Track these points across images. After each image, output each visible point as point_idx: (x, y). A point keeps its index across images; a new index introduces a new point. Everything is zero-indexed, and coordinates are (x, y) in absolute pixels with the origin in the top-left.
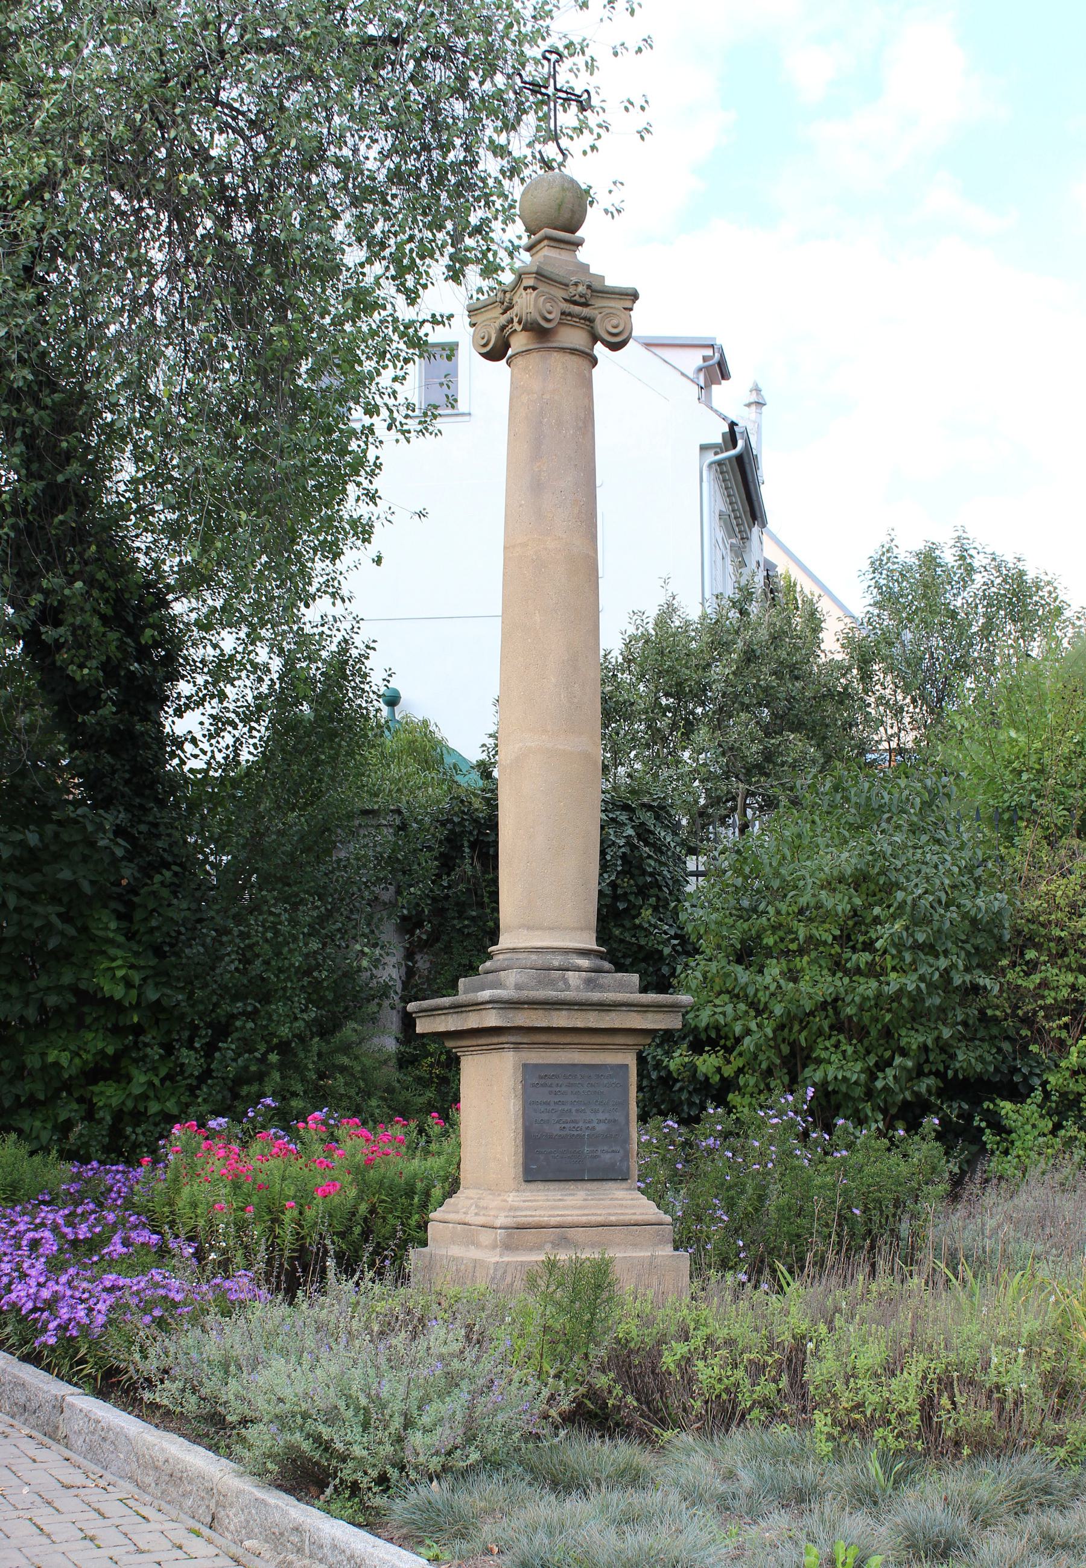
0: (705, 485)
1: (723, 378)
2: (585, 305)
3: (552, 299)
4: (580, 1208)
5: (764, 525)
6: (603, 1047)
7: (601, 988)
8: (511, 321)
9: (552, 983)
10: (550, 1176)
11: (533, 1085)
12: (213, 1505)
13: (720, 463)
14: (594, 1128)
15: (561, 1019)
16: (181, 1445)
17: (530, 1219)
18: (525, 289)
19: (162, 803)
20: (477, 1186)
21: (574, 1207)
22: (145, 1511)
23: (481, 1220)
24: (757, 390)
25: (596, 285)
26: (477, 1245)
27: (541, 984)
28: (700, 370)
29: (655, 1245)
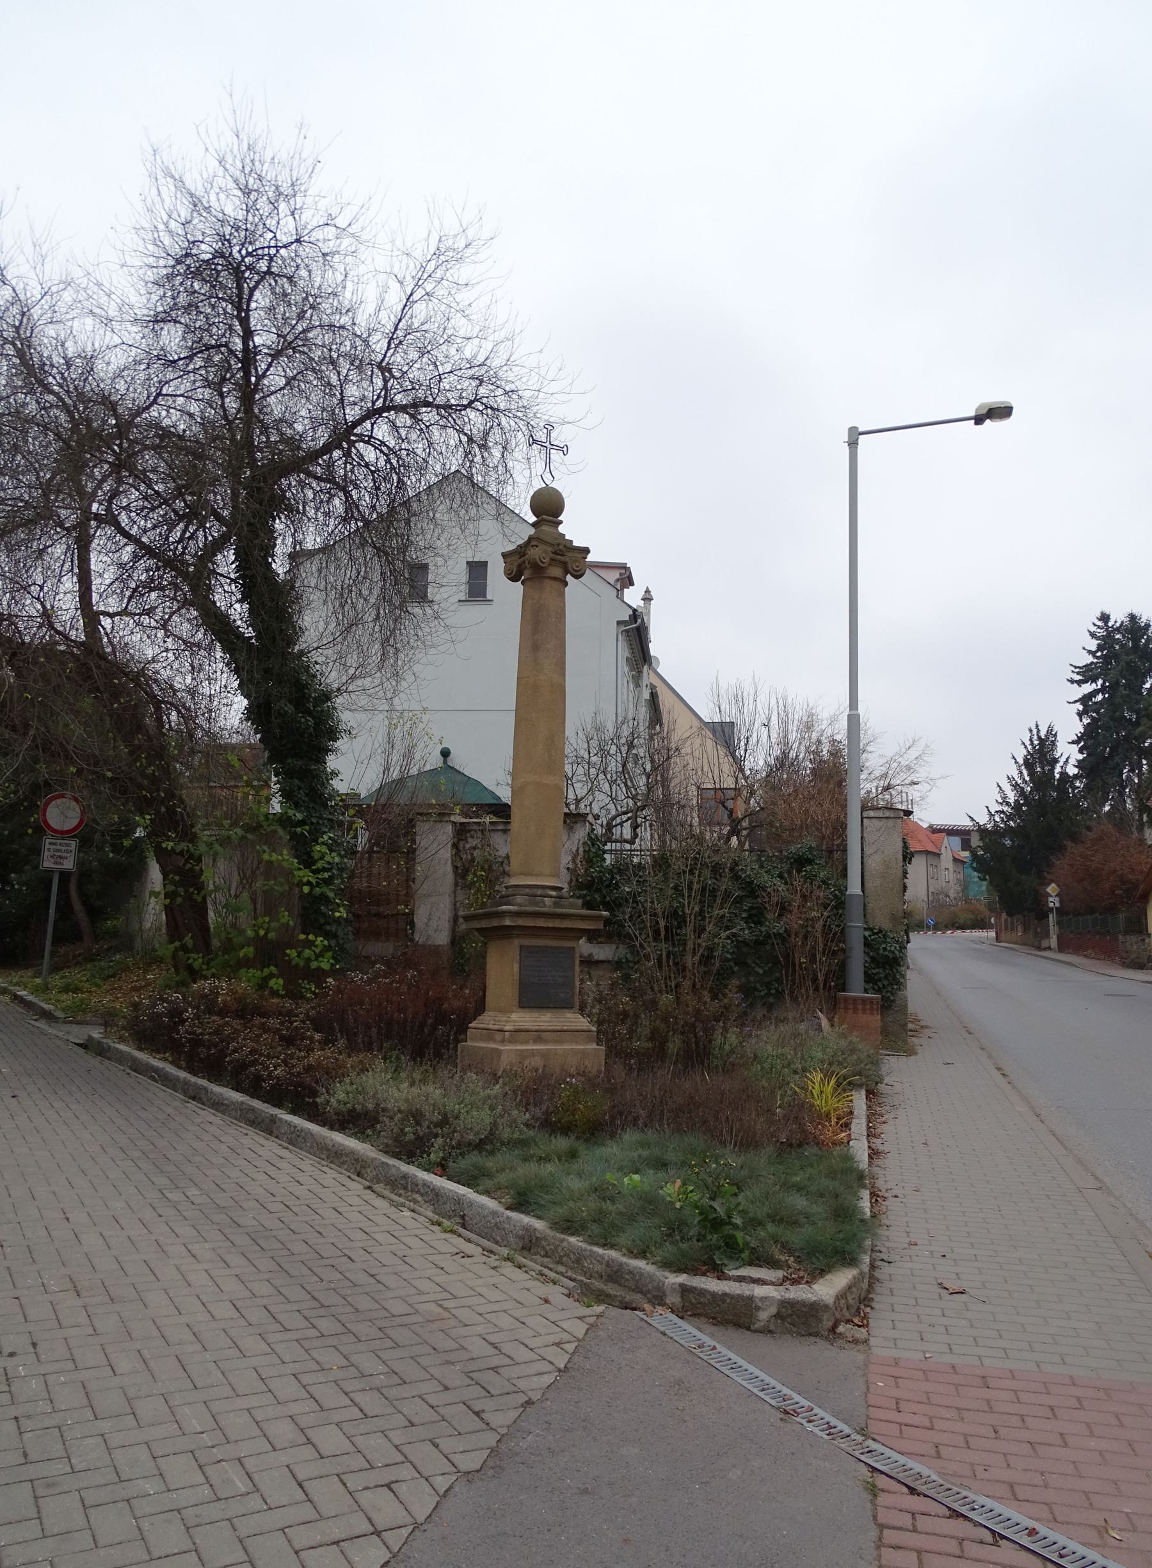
3: (545, 552)
5: (650, 664)
9: (536, 904)
12: (358, 1167)
13: (627, 631)
15: (541, 923)
22: (324, 1169)
23: (496, 1027)
24: (647, 591)
26: (494, 1041)
29: (587, 1043)
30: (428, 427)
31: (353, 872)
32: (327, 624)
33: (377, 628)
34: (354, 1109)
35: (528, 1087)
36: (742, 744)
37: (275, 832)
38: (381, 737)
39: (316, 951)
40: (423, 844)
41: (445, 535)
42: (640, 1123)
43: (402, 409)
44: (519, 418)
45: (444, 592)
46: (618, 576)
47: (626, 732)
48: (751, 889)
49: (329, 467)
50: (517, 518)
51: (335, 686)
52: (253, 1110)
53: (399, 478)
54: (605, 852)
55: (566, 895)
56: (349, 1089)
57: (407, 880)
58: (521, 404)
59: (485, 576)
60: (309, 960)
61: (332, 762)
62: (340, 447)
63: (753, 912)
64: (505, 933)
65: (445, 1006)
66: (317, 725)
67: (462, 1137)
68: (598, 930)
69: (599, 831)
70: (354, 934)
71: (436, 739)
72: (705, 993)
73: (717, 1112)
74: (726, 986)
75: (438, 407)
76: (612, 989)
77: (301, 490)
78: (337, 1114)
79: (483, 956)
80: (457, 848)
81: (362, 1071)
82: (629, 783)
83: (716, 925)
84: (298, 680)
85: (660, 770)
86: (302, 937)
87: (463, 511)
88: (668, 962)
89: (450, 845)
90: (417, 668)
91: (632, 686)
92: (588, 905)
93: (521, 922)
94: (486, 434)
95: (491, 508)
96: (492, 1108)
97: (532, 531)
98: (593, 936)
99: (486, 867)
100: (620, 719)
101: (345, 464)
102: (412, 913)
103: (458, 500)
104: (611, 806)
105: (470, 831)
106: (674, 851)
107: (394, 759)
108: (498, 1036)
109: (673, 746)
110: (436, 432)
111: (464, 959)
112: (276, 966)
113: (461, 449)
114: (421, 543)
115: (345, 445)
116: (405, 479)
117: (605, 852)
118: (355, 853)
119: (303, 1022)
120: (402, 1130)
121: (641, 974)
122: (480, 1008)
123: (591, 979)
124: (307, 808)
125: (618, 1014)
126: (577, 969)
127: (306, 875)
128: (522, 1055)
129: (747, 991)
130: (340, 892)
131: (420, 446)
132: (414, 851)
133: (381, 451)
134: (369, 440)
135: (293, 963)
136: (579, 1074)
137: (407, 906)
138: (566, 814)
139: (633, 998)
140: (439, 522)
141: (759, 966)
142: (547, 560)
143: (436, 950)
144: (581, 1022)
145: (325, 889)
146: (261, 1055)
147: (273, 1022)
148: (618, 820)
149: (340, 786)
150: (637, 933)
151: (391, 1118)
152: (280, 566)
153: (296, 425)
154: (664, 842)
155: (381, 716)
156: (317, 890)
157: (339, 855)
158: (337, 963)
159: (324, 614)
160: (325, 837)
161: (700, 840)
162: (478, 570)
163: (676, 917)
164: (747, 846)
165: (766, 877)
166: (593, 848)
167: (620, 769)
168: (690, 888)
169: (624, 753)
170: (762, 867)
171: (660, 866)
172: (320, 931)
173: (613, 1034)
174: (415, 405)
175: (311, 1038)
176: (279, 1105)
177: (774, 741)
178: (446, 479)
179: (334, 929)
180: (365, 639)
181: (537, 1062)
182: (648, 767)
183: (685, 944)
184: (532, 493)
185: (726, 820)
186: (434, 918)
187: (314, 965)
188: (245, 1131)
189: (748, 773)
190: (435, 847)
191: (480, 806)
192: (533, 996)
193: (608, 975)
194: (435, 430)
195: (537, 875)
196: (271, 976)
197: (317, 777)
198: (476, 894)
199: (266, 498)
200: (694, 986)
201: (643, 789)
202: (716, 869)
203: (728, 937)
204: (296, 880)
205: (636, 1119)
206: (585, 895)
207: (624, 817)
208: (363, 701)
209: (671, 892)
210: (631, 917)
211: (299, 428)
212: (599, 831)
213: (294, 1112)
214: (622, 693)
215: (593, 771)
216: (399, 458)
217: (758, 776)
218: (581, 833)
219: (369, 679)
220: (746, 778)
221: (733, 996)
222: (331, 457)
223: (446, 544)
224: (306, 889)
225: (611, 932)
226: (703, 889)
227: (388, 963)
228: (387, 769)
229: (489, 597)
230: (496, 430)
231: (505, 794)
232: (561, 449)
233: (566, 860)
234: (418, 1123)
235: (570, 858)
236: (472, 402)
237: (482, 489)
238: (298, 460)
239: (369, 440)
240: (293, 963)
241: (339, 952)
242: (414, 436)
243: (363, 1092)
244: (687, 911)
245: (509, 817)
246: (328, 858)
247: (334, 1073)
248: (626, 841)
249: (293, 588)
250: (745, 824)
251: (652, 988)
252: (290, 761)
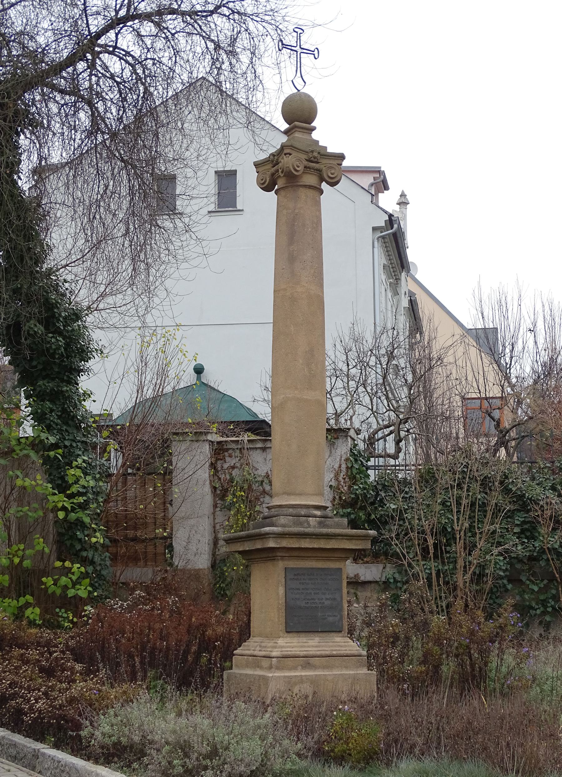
0: (376, 250)
1: (385, 189)
3: (299, 160)
4: (316, 647)
5: (408, 271)
6: (328, 559)
7: (328, 526)
8: (277, 171)
9: (301, 524)
10: (300, 630)
11: (291, 579)
13: (383, 237)
14: (324, 603)
15: (306, 544)
16: (107, 772)
17: (289, 653)
18: (285, 154)
19: (78, 428)
20: (260, 635)
21: (313, 646)
24: (403, 195)
25: (322, 152)
26: (261, 668)
27: (296, 524)
28: (372, 185)
29: (357, 667)
30: (173, 35)
31: (108, 495)
32: (76, 241)
33: (127, 243)
34: (120, 742)
35: (298, 715)
36: (507, 350)
37: (27, 456)
38: (134, 355)
39: (72, 578)
40: (179, 465)
41: (195, 145)
42: (417, 750)
43: (148, 17)
44: (267, 22)
45: (195, 204)
46: (372, 181)
47: (385, 342)
48: (523, 503)
49: (73, 80)
50: (268, 126)
51: (85, 304)
52: (15, 745)
53: (146, 89)
54: (368, 468)
55: (330, 514)
56: (114, 721)
57: (164, 503)
58: (268, 8)
60: (66, 587)
61: (85, 383)
62: (83, 58)
63: (526, 526)
64: (269, 555)
65: (209, 632)
66: (67, 345)
67: (233, 768)
68: (364, 550)
69: (361, 446)
70: (111, 560)
71: (190, 356)
72: (479, 612)
73: (498, 737)
74: (500, 605)
75: (183, 14)
76: (381, 612)
77: (50, 106)
78: (102, 747)
79: (246, 579)
80: (215, 468)
81: (127, 701)
82: (390, 395)
83: (487, 541)
84: (47, 300)
85: (422, 382)
86: (58, 564)
87: (212, 120)
88: (438, 581)
89: (207, 464)
90: (168, 283)
91: (389, 294)
92: (353, 524)
93: (285, 543)
94: (233, 40)
95: (241, 116)
96: (263, 738)
97: (284, 139)
98: (358, 556)
99: (246, 486)
100: (379, 329)
101: (90, 75)
102: (170, 537)
103: (206, 109)
104: (372, 420)
105: (227, 450)
106: (441, 465)
107: (148, 378)
108: (265, 663)
109: (435, 355)
110: (182, 40)
111: (226, 584)
112: (32, 595)
113: (208, 57)
114: (171, 155)
115: (89, 56)
116: (152, 89)
117: (368, 468)
118: (110, 475)
119: (63, 652)
120: (170, 763)
121: (411, 594)
122: (245, 633)
123: (358, 602)
124: (60, 431)
125: (388, 637)
126: (345, 590)
127: (60, 500)
128: (290, 682)
129: (523, 609)
130: (96, 517)
131: (167, 54)
132: (171, 472)
133: (127, 62)
134: (114, 50)
135: (50, 591)
136: (350, 700)
137: (165, 529)
138: (328, 430)
139: (404, 620)
140: (187, 132)
141: (533, 583)
142: (300, 169)
143: (196, 575)
144: (352, 647)
145: (80, 514)
146: (21, 687)
147: (33, 654)
148: (380, 434)
149: (92, 407)
150: (405, 552)
151: (158, 750)
152: (25, 183)
153: (38, 38)
154: (428, 456)
155: (133, 334)
156: (73, 516)
157: (94, 478)
158: (95, 589)
159: (72, 231)
160: (80, 460)
161: (467, 453)
162: (227, 179)
163: (446, 535)
164: (515, 459)
165: (539, 490)
166: (356, 464)
167: (381, 381)
168: (459, 504)
169: (384, 364)
170: (533, 479)
171: (427, 482)
172: (77, 557)
173: (384, 658)
174: (160, 13)
175: (72, 669)
176: (41, 738)
177: (540, 347)
178: (193, 86)
179: (90, 556)
180: (114, 255)
181: (307, 689)
182: (410, 378)
183: (456, 562)
184: (283, 99)
185: (493, 431)
186: (194, 542)
187: (71, 593)
188: (7, 767)
189: (514, 380)
190: (192, 467)
191: (237, 424)
192: (300, 620)
193: (375, 596)
194: (180, 37)
195: (300, 495)
196: (27, 605)
197: (69, 398)
198: (235, 515)
199: (11, 114)
200: (467, 606)
201: (405, 401)
202: (485, 483)
203: (500, 554)
204: (51, 506)
205: (413, 747)
206: (349, 514)
207: (387, 431)
208: (115, 319)
209: (438, 508)
210: (398, 535)
211: (41, 40)
212: (361, 446)
213: (56, 746)
214: (380, 302)
215: (352, 384)
216: (145, 68)
217: (526, 384)
218: (343, 449)
219: (120, 296)
220: (513, 386)
221: (509, 616)
222: (75, 70)
223: (195, 154)
224: (61, 515)
225: (379, 552)
226: (473, 504)
227: (147, 589)
228: (140, 388)
229: (239, 207)
230: (244, 35)
231: (263, 412)
232: (311, 52)
233: (329, 477)
234: (186, 755)
235: (332, 475)
236: (218, 7)
237: (231, 96)
238: (40, 73)
239: (114, 50)
240: (50, 591)
241: (97, 579)
242: (160, 44)
243: (127, 723)
244: (456, 527)
245: (270, 435)
246: (82, 482)
247: (98, 706)
248: (389, 456)
249: (39, 205)
250: (513, 434)
251: (422, 609)
252: (41, 383)
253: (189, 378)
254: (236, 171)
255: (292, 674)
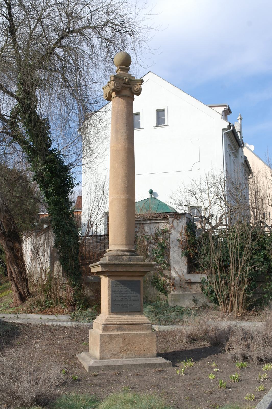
2: (129, 84)
7: (133, 260)
13: (228, 133)
14: (131, 298)
15: (119, 269)
17: (111, 323)
21: (124, 319)
59: (164, 115)
229: (166, 124)
253: (148, 196)
254: (164, 109)
255: (112, 333)
